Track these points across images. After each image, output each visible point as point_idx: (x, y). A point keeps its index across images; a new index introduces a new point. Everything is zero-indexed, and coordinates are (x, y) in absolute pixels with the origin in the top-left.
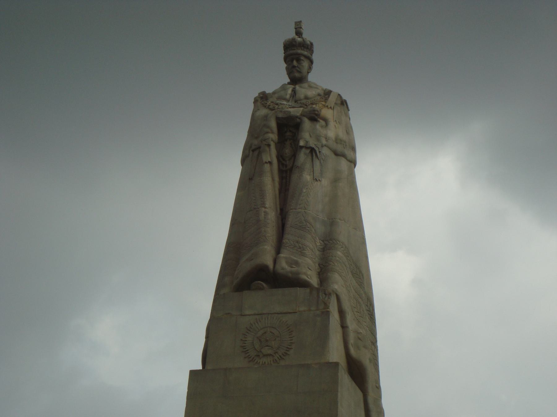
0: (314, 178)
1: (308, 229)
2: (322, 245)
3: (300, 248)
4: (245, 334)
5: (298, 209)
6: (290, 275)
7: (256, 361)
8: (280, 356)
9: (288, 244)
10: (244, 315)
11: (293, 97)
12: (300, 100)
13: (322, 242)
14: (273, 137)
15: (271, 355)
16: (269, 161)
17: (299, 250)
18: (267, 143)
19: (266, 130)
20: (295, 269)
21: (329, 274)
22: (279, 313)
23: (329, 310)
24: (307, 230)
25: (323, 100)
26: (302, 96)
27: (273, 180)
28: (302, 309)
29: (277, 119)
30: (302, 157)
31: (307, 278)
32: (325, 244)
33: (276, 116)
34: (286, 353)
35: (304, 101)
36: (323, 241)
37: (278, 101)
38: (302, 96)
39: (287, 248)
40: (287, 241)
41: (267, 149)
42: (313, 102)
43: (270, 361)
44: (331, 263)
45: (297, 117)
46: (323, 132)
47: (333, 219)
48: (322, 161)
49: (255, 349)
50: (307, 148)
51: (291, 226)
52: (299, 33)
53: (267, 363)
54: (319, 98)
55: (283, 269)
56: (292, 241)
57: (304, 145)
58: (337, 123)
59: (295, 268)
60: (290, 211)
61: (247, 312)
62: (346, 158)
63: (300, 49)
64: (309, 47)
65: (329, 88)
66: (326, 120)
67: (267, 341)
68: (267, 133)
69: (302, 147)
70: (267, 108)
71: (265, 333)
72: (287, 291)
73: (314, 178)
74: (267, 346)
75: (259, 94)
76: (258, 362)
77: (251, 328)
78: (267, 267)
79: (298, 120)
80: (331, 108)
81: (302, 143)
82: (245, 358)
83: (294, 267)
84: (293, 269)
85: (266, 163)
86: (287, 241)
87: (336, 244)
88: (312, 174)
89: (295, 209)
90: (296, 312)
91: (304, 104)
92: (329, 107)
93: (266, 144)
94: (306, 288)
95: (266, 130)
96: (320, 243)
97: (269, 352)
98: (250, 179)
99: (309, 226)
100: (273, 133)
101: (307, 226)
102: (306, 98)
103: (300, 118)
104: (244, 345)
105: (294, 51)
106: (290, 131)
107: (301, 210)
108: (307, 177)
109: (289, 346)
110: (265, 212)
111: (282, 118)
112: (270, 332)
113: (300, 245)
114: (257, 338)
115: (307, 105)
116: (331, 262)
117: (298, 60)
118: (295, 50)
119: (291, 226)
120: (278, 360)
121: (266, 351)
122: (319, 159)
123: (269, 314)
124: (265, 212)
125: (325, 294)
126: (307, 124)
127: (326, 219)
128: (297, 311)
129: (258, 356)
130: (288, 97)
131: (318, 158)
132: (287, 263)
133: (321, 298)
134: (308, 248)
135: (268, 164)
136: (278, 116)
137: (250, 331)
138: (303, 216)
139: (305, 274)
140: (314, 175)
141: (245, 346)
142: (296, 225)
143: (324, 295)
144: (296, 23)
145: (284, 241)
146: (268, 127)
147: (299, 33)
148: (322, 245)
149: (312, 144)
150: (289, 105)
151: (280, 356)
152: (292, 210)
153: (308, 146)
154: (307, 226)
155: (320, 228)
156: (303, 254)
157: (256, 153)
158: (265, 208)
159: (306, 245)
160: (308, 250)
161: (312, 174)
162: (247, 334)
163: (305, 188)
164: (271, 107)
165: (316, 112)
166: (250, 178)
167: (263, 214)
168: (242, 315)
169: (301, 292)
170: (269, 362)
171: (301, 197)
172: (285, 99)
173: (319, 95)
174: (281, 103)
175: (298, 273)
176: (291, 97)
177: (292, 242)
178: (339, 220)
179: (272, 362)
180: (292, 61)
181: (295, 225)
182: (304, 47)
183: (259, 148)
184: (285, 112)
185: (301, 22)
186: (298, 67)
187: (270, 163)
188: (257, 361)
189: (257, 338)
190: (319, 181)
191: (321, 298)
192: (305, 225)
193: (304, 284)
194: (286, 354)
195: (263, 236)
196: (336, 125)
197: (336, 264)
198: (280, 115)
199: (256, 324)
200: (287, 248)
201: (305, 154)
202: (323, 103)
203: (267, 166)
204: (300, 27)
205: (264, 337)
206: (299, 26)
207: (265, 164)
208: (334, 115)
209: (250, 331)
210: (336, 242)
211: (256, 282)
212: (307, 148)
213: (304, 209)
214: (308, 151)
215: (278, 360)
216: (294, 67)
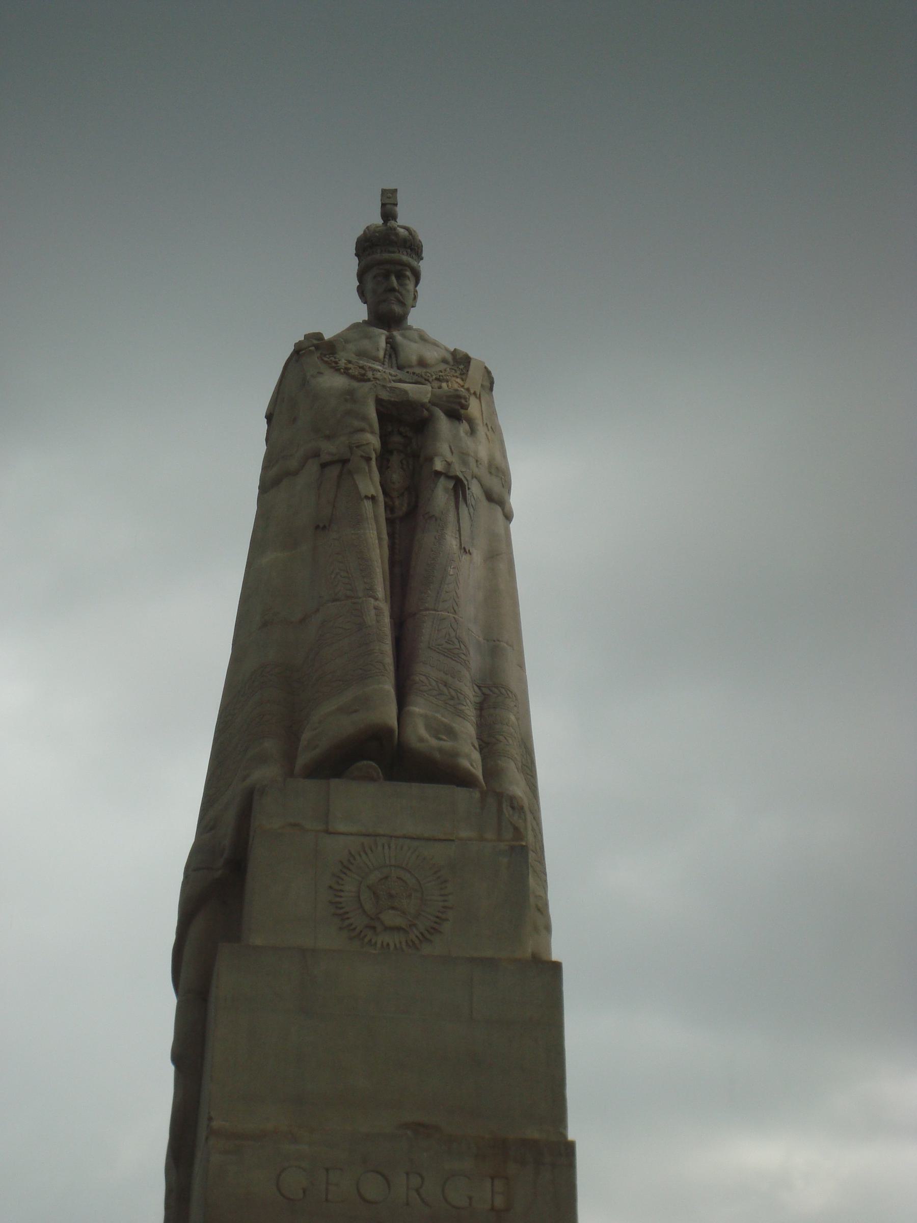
0: (461, 545)
1: (463, 657)
2: (477, 696)
3: (452, 698)
4: (338, 877)
5: (441, 611)
6: (437, 756)
7: (366, 940)
8: (422, 934)
9: (426, 685)
10: (331, 833)
11: (390, 356)
12: (411, 366)
13: (476, 688)
14: (373, 440)
15: (403, 929)
16: (372, 495)
17: (452, 702)
18: (364, 454)
19: (357, 424)
20: (447, 744)
21: (499, 762)
22: (414, 838)
23: (524, 844)
24: (463, 659)
25: (457, 374)
26: (414, 359)
27: (380, 539)
28: (464, 834)
29: (379, 402)
30: (441, 496)
31: (471, 768)
32: (484, 694)
33: (377, 396)
34: (434, 929)
35: (418, 370)
36: (479, 687)
37: (361, 362)
38: (414, 359)
39: (425, 694)
40: (423, 678)
41: (364, 464)
42: (440, 376)
43: (400, 943)
44: (501, 738)
45: (423, 405)
46: (468, 442)
47: (494, 641)
48: (471, 510)
49: (364, 912)
50: (448, 477)
51: (429, 648)
52: (388, 214)
53: (392, 947)
54: (443, 366)
55: (421, 740)
56: (433, 679)
57: (443, 471)
58: (488, 430)
59: (444, 740)
60: (424, 613)
61: (341, 828)
62: (503, 510)
63: (405, 253)
64: (413, 247)
65: (466, 348)
66: (471, 422)
67: (391, 896)
68: (362, 430)
69: (438, 474)
70: (341, 374)
71: (386, 878)
72: (431, 789)
73: (461, 545)
74: (393, 908)
75: (307, 337)
76: (373, 941)
77: (352, 864)
78: (390, 731)
79: (426, 413)
80: (475, 393)
81: (439, 466)
82: (341, 929)
83: (444, 737)
84: (442, 743)
85: (367, 497)
86: (423, 678)
87: (506, 697)
88: (458, 537)
89: (435, 610)
90: (453, 840)
91: (421, 376)
92: (472, 391)
93: (362, 456)
94: (471, 790)
95: (357, 424)
96: (475, 692)
97: (399, 921)
98: (317, 527)
99: (464, 652)
100: (373, 433)
101: (462, 651)
102: (422, 363)
103: (427, 410)
104: (338, 899)
105: (386, 256)
106: (400, 433)
107: (447, 614)
108: (452, 542)
109: (440, 915)
110: (375, 608)
111: (390, 402)
112: (397, 878)
113: (453, 693)
114: (369, 887)
115: (431, 380)
116: (502, 735)
117: (400, 276)
118: (394, 252)
119: (429, 648)
120: (417, 942)
121: (391, 918)
122: (467, 506)
123: (391, 837)
124: (375, 608)
125: (513, 808)
126: (444, 424)
127: (481, 639)
128: (454, 838)
129: (374, 928)
130: (381, 354)
131: (466, 503)
132: (428, 727)
133: (507, 816)
134: (468, 701)
135: (370, 500)
136: (380, 397)
137: (348, 869)
138: (452, 628)
139: (468, 757)
140: (462, 538)
141: (341, 903)
142: (439, 645)
143: (509, 808)
144: (384, 192)
145: (417, 678)
146: (365, 418)
147: (388, 214)
148: (477, 696)
149: (458, 470)
150: (391, 375)
151: (422, 934)
152: (428, 612)
153: (451, 474)
154: (462, 651)
155: (475, 660)
156: (460, 714)
157: (334, 471)
158: (376, 599)
159: (463, 693)
160: (468, 706)
161: (457, 536)
162: (342, 876)
163: (452, 567)
164: (355, 371)
165: (463, 401)
166: (321, 525)
167: (373, 612)
168: (327, 832)
169: (461, 793)
170: (398, 945)
171: (446, 586)
172: (376, 359)
173: (444, 361)
174: (370, 367)
175: (455, 754)
176: (387, 356)
177: (434, 683)
178: (505, 644)
179: (404, 947)
180: (387, 276)
181: (437, 647)
182: (411, 250)
183: (344, 462)
184: (393, 389)
185: (396, 190)
186: (399, 292)
187: (373, 498)
188: (371, 940)
189: (369, 887)
190: (468, 555)
191: (507, 816)
192: (458, 649)
193: (463, 780)
194: (434, 930)
195: (377, 662)
196: (488, 434)
197: (511, 741)
198: (384, 395)
199: (364, 856)
200: (425, 694)
201: (446, 490)
202: (459, 380)
203: (368, 504)
204: (392, 202)
205: (383, 887)
206: (391, 201)
207: (365, 501)
208: (482, 411)
209: (348, 869)
210: (505, 692)
211: (365, 762)
212: (448, 477)
213: (453, 614)
214: (451, 484)
215: (417, 942)
216: (393, 290)
